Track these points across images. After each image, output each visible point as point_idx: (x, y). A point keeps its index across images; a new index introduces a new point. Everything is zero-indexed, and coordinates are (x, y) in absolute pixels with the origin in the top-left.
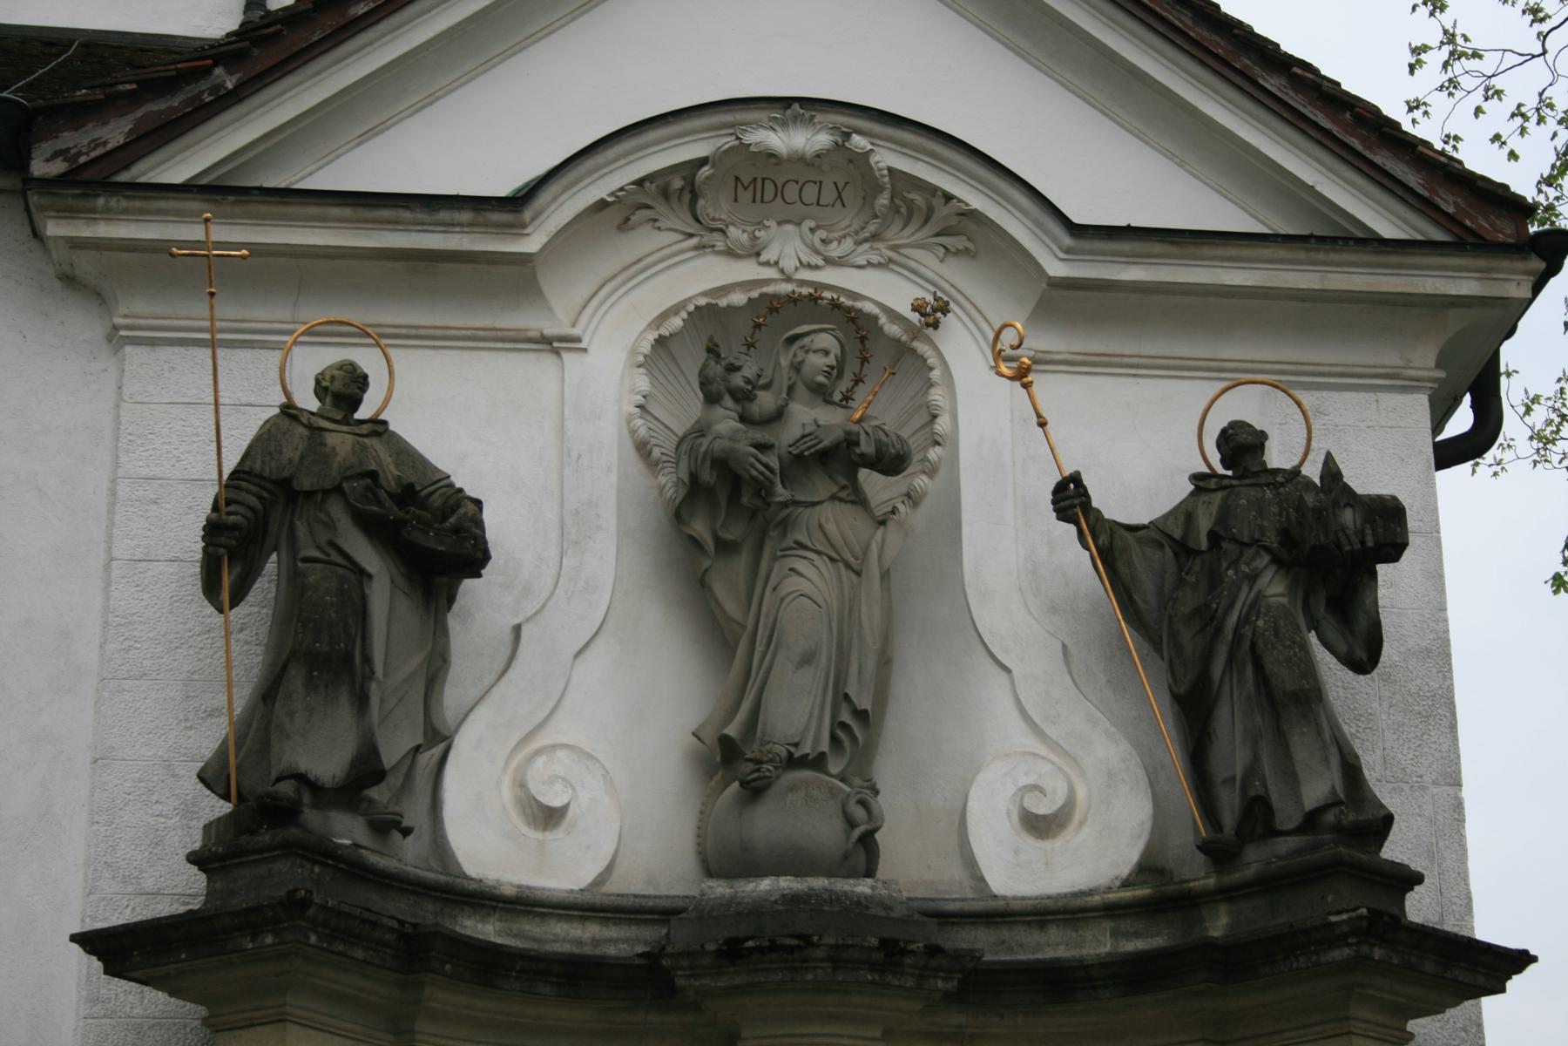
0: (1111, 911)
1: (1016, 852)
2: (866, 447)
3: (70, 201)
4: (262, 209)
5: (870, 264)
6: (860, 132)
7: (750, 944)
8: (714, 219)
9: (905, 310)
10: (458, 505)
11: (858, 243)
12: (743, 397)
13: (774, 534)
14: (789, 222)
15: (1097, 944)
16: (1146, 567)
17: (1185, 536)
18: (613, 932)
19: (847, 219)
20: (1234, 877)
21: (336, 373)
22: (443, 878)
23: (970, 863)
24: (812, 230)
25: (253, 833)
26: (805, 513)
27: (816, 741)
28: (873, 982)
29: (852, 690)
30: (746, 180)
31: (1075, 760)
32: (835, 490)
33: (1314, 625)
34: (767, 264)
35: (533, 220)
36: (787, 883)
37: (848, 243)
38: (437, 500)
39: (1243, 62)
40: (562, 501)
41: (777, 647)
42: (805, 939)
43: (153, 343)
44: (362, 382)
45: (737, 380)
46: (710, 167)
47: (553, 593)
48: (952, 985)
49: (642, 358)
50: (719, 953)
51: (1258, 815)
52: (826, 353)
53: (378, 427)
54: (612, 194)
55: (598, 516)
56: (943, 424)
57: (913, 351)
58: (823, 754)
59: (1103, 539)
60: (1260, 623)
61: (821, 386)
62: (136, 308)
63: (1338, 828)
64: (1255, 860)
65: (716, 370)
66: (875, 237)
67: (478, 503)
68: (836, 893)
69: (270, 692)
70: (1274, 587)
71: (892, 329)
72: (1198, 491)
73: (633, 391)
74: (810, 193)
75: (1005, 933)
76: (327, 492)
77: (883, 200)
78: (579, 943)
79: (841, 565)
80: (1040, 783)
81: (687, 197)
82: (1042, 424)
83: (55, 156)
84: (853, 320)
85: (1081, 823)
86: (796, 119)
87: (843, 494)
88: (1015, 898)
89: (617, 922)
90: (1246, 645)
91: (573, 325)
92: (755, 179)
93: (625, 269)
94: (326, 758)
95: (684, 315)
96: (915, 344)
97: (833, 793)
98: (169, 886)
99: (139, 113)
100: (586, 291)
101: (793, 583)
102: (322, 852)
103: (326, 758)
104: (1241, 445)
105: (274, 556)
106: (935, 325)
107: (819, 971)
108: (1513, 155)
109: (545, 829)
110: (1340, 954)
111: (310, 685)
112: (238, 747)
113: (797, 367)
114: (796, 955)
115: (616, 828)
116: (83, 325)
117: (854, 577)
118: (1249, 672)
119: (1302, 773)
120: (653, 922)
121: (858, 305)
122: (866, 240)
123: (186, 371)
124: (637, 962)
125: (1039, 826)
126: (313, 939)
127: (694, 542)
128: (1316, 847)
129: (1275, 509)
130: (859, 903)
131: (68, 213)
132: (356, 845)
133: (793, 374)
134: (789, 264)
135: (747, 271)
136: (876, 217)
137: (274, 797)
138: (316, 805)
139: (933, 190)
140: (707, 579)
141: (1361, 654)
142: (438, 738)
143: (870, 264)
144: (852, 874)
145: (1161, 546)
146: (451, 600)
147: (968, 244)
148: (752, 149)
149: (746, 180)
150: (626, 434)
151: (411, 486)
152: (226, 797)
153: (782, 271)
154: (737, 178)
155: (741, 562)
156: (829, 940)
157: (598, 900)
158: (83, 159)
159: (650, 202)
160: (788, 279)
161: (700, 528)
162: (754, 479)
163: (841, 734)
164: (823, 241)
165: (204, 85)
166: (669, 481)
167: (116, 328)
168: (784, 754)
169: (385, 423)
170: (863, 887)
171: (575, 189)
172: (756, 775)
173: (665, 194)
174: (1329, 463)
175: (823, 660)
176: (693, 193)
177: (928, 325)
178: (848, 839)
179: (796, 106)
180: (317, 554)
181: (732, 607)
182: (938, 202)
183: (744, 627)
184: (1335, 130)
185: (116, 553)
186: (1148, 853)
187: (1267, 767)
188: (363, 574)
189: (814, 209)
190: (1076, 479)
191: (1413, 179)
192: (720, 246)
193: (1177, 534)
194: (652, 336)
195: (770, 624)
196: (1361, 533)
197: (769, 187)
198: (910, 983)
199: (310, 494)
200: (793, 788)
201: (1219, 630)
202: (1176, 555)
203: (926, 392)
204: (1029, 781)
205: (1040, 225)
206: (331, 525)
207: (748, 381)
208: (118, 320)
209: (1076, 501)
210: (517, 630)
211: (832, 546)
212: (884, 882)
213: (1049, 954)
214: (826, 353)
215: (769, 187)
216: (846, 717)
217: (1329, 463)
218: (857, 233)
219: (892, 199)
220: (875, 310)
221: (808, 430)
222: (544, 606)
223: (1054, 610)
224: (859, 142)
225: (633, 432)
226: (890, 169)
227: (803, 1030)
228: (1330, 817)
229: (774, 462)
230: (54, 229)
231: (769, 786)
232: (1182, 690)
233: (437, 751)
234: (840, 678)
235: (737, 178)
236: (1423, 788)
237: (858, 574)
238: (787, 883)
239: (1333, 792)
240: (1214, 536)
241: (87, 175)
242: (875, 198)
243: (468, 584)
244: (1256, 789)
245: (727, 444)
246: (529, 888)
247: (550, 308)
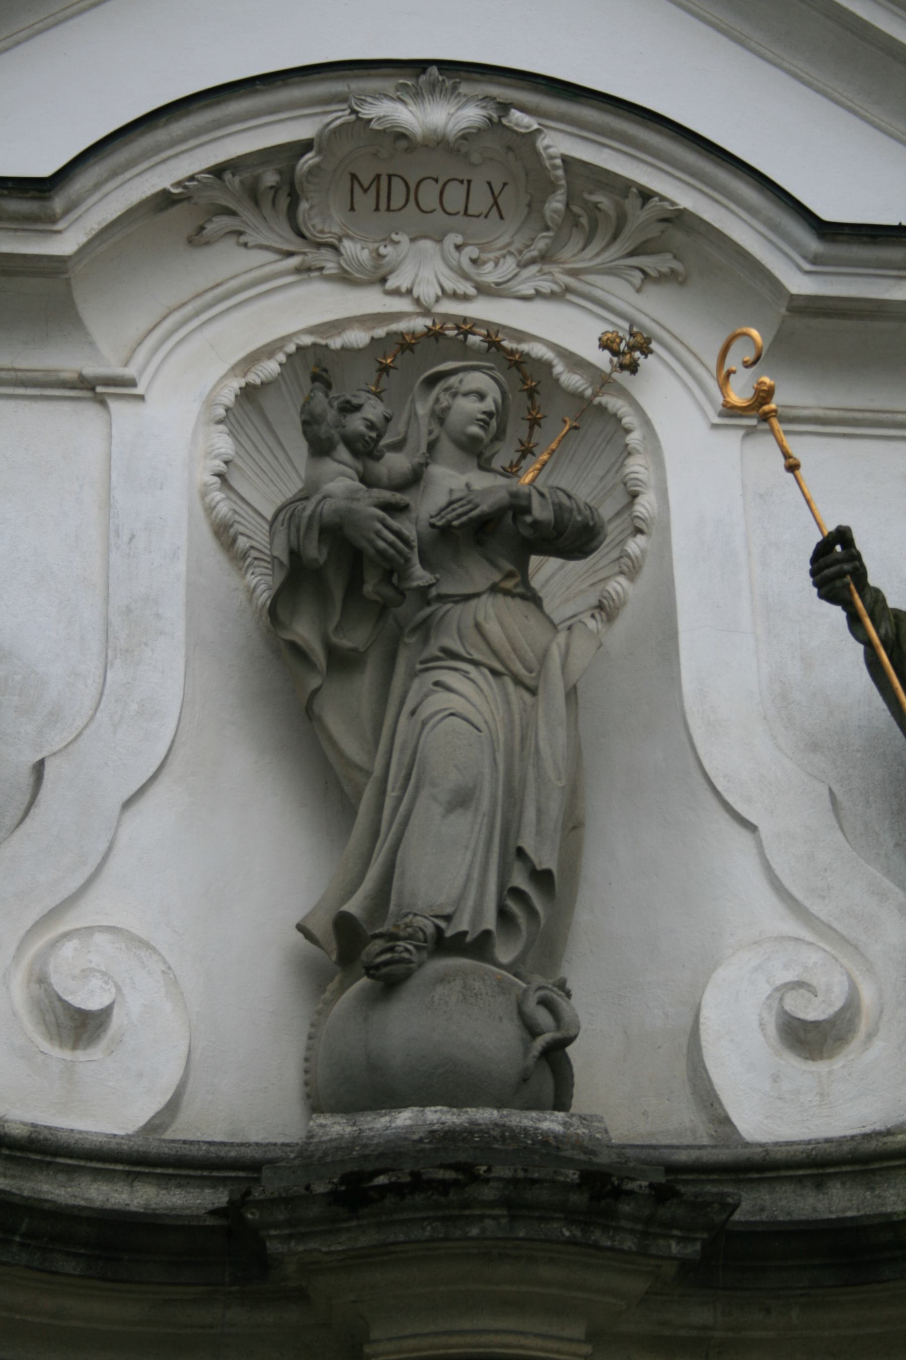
1: (776, 1079)
6: (523, 109)
7: (382, 1180)
11: (523, 265)
12: (365, 449)
14: (425, 237)
19: (505, 234)
24: (458, 248)
26: (456, 611)
27: (477, 914)
28: (572, 1242)
29: (528, 843)
30: (366, 180)
31: (856, 948)
32: (497, 577)
34: (396, 292)
35: (67, 211)
36: (437, 1116)
37: (509, 265)
40: (108, 595)
41: (417, 788)
42: (466, 1168)
45: (356, 424)
46: (313, 159)
47: (92, 718)
48: (693, 1250)
49: (221, 412)
50: (334, 1197)
52: (481, 396)
54: (178, 184)
55: (158, 616)
56: (646, 505)
57: (602, 409)
58: (487, 933)
61: (475, 439)
66: (544, 258)
68: (511, 1129)
71: (572, 380)
73: (210, 454)
74: (455, 196)
77: (556, 203)
79: (508, 681)
80: (806, 978)
81: (284, 202)
85: (870, 1036)
86: (433, 87)
87: (509, 584)
89: (183, 1182)
91: (126, 365)
92: (378, 177)
93: (199, 295)
95: (282, 357)
96: (604, 399)
97: (502, 987)
100: (144, 324)
101: (441, 700)
107: (488, 1222)
109: (74, 1047)
113: (440, 417)
114: (453, 1196)
117: (526, 696)
121: (525, 347)
122: (533, 261)
124: (210, 1222)
125: (809, 1039)
127: (298, 652)
130: (545, 1143)
133: (435, 427)
134: (427, 291)
135: (371, 301)
136: (547, 229)
140: (316, 708)
143: (539, 294)
144: (536, 1105)
147: (676, 265)
148: (374, 125)
149: (366, 180)
153: (417, 301)
154: (354, 177)
155: (365, 682)
156: (503, 1171)
157: (153, 1146)
159: (232, 205)
161: (304, 631)
162: (381, 553)
163: (513, 906)
164: (474, 261)
166: (263, 583)
168: (430, 930)
170: (551, 1123)
171: (128, 175)
172: (387, 956)
173: (253, 194)
176: (291, 193)
177: (622, 367)
178: (527, 1050)
182: (632, 203)
183: (368, 774)
190: (843, 536)
192: (331, 268)
194: (236, 384)
195: (406, 760)
197: (398, 188)
198: (629, 1243)
200: (443, 979)
203: (622, 465)
204: (790, 976)
205: (775, 228)
207: (371, 426)
209: (847, 567)
210: (39, 768)
211: (495, 653)
212: (582, 1118)
214: (481, 396)
215: (398, 188)
216: (520, 880)
218: (520, 252)
219: (567, 206)
220: (548, 354)
221: (456, 496)
223: (814, 747)
225: (210, 509)
226: (567, 160)
231: (408, 975)
234: (510, 827)
235: (354, 177)
237: (533, 692)
238: (437, 1116)
242: (544, 202)
245: (343, 504)
246: (49, 1128)
247: (92, 344)
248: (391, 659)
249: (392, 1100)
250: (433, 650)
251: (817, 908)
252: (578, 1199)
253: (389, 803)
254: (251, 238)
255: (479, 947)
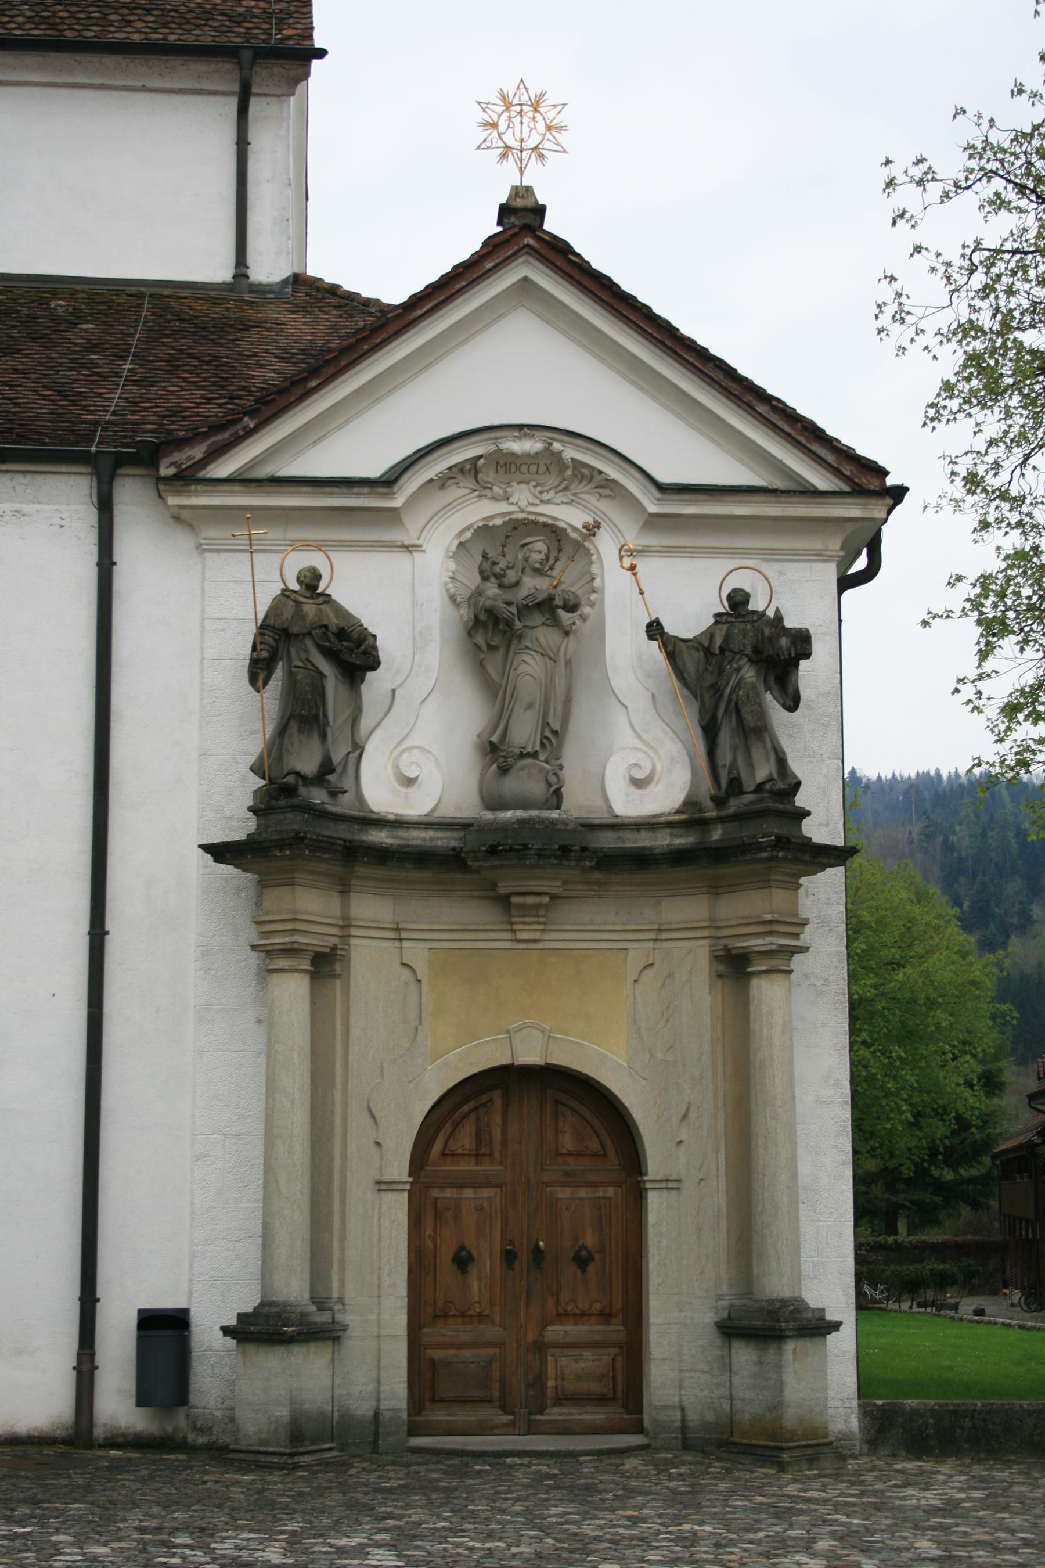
0: (670, 824)
1: (627, 795)
2: (558, 601)
3: (179, 488)
4: (269, 489)
5: (563, 502)
8: (486, 482)
9: (580, 526)
10: (365, 640)
11: (557, 493)
13: (515, 641)
15: (663, 841)
16: (691, 661)
17: (709, 646)
18: (440, 834)
19: (552, 480)
20: (724, 813)
21: (308, 574)
22: (361, 814)
23: (606, 799)
25: (277, 799)
29: (550, 721)
30: (502, 462)
32: (544, 620)
33: (768, 688)
34: (512, 503)
36: (520, 814)
37: (552, 493)
38: (355, 635)
39: (748, 398)
43: (218, 551)
44: (318, 577)
45: (497, 569)
47: (410, 673)
48: (593, 863)
50: (487, 851)
51: (735, 786)
52: (540, 552)
53: (327, 598)
56: (597, 583)
59: (670, 648)
60: (741, 692)
62: (211, 533)
63: (771, 792)
64: (734, 805)
65: (487, 566)
66: (566, 489)
67: (375, 637)
69: (282, 732)
70: (749, 673)
71: (574, 535)
72: (716, 623)
75: (621, 834)
76: (304, 635)
77: (569, 472)
78: (424, 839)
81: (473, 472)
82: (642, 593)
83: (171, 465)
84: (554, 532)
85: (658, 782)
86: (526, 435)
87: (548, 623)
88: (626, 817)
89: (442, 830)
90: (733, 703)
93: (443, 508)
94: (307, 763)
95: (472, 531)
98: (239, 827)
99: (209, 442)
101: (523, 668)
102: (309, 809)
103: (307, 763)
104: (738, 600)
105: (281, 663)
106: (594, 535)
108: (935, 357)
110: (764, 855)
111: (301, 731)
112: (269, 756)
115: (441, 784)
116: (184, 540)
118: (734, 718)
119: (756, 766)
120: (458, 830)
121: (557, 523)
123: (237, 565)
125: (638, 783)
126: (307, 852)
127: (478, 647)
128: (761, 800)
129: (751, 634)
130: (552, 823)
131: (178, 493)
132: (323, 803)
134: (523, 504)
135: (503, 507)
137: (286, 784)
138: (305, 785)
139: (593, 468)
141: (790, 703)
142: (358, 748)
143: (563, 502)
145: (698, 650)
146: (362, 681)
149: (502, 462)
150: (444, 591)
151: (343, 629)
152: (264, 778)
155: (500, 655)
157: (433, 820)
158: (184, 467)
160: (523, 511)
161: (480, 639)
163: (545, 741)
165: (239, 426)
167: (201, 545)
169: (329, 596)
170: (555, 814)
173: (462, 471)
174: (777, 610)
175: (537, 706)
178: (548, 791)
179: (526, 429)
180: (300, 664)
181: (495, 676)
182: (595, 474)
183: (501, 686)
184: (793, 433)
185: (205, 656)
186: (688, 796)
187: (740, 762)
188: (322, 675)
189: (536, 476)
191: (830, 458)
193: (706, 644)
194: (456, 542)
196: (789, 650)
199: (296, 635)
200: (522, 769)
201: (721, 696)
202: (705, 654)
204: (634, 761)
205: (645, 487)
206: (306, 651)
207: (502, 570)
208: (202, 541)
210: (394, 691)
211: (543, 648)
213: (641, 844)
214: (540, 552)
215: (513, 467)
216: (548, 733)
217: (777, 610)
222: (406, 680)
223: (649, 676)
224: (557, 446)
225: (447, 591)
226: (573, 459)
227: (526, 883)
228: (768, 786)
229: (514, 610)
230: (173, 501)
232: (704, 723)
233: (357, 753)
234: (545, 715)
236: (823, 760)
237: (555, 661)
238: (520, 814)
239: (771, 774)
240: (721, 648)
241: (186, 473)
243: (370, 675)
244: (734, 774)
248: (508, 647)
249: (505, 807)
250: (522, 646)
251: (645, 737)
252: (558, 853)
253: (506, 702)
254: (461, 485)
255: (534, 755)
